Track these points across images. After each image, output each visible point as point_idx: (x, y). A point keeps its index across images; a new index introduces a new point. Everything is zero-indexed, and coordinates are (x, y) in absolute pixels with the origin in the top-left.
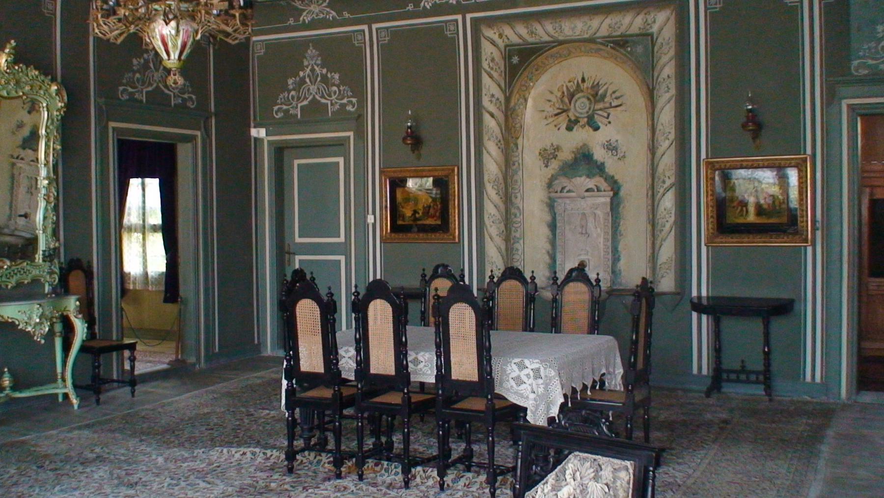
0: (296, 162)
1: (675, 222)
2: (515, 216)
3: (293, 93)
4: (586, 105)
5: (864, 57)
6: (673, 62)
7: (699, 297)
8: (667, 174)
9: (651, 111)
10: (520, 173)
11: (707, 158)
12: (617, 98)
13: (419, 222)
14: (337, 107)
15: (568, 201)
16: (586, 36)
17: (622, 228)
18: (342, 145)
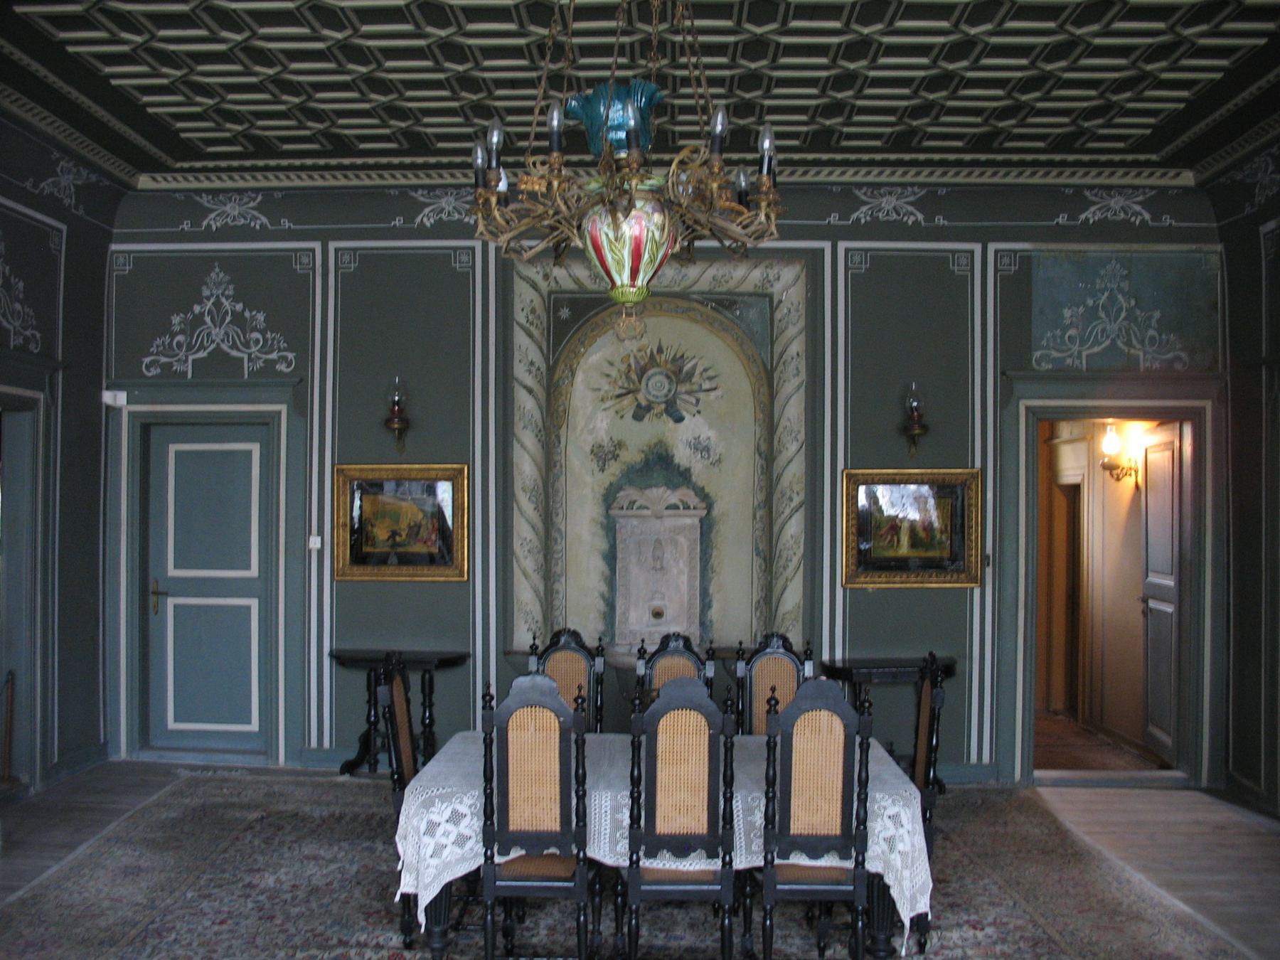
0: (173, 448)
1: (804, 555)
2: (556, 540)
4: (661, 385)
5: (1048, 347)
6: (802, 337)
7: (832, 660)
8: (796, 488)
9: (765, 399)
11: (846, 467)
12: (710, 379)
13: (400, 550)
14: (260, 364)
15: (635, 522)
16: (676, 289)
17: (714, 561)
18: (267, 424)
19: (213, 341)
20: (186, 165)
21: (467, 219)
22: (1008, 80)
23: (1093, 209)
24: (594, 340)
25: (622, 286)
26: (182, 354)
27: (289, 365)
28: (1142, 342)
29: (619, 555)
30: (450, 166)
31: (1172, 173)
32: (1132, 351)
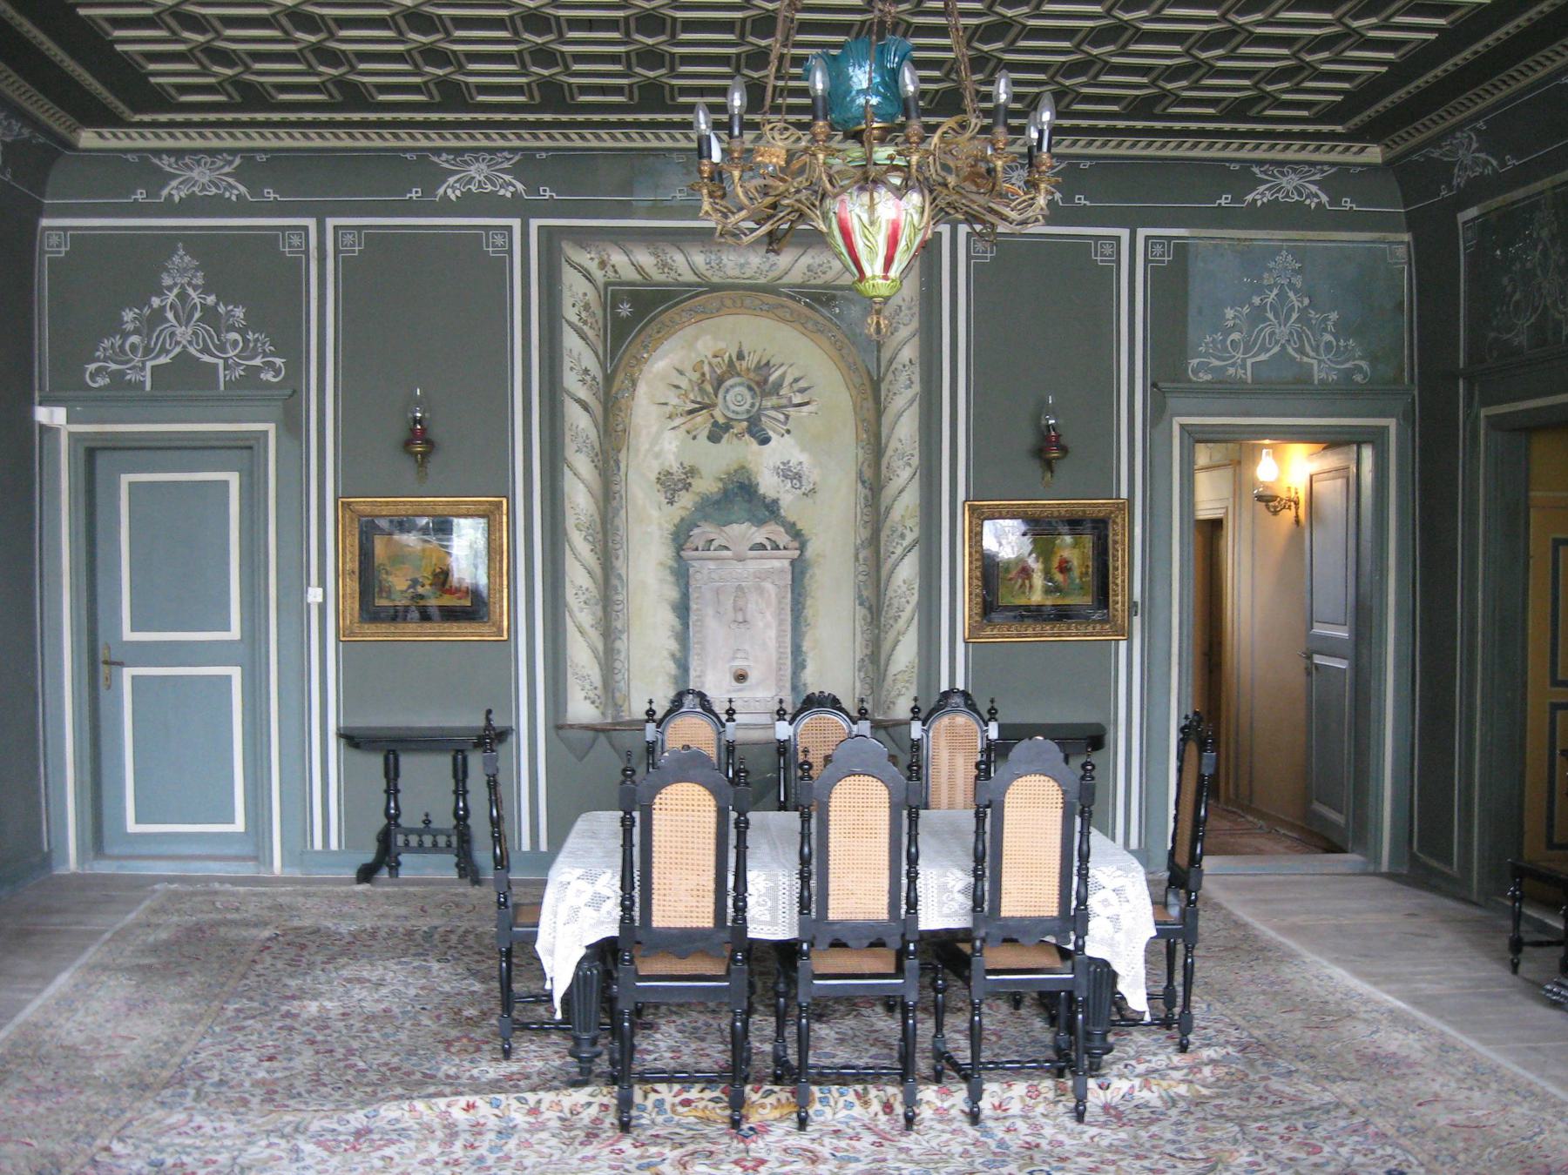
1: (918, 603)
3: (135, 339)
4: (741, 400)
5: (1206, 354)
6: (916, 340)
9: (870, 415)
10: (623, 513)
12: (802, 391)
14: (239, 372)
15: (712, 565)
16: (762, 281)
17: (808, 613)
19: (178, 343)
20: (147, 118)
21: (502, 192)
22: (1190, 34)
23: (1261, 188)
24: (660, 341)
25: (874, 278)
26: (137, 361)
27: (277, 372)
28: (1316, 349)
29: (693, 606)
30: (588, 125)
31: (1357, 146)
32: (1305, 359)
